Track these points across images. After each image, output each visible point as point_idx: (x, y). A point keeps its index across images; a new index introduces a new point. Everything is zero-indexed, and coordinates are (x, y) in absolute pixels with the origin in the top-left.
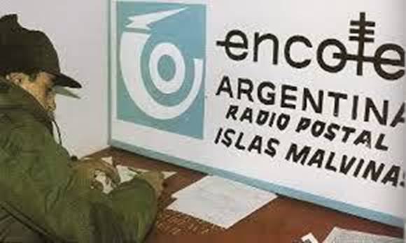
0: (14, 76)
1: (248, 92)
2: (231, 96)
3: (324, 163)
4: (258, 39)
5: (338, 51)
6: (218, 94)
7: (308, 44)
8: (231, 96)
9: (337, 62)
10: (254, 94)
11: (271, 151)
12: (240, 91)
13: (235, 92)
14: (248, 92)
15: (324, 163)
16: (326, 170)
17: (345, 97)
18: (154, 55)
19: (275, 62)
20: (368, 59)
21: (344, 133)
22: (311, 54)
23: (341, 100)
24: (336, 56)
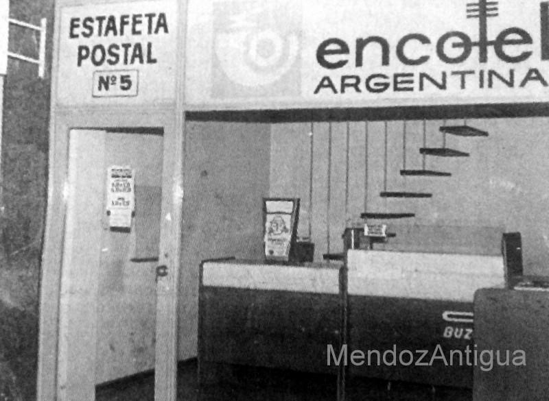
0: (325, 162)
1: (356, 86)
2: (335, 91)
3: (145, 58)
4: (361, 44)
5: (458, 40)
6: (79, 64)
7: (424, 40)
8: (335, 91)
9: (459, 52)
10: (362, 86)
11: (125, 79)
12: (344, 86)
13: (338, 86)
14: (356, 86)
15: (145, 58)
16: (149, 65)
17: (472, 72)
18: (496, 123)
19: (481, 86)
20: (475, 44)
21: (147, 19)
22: (430, 50)
23: (467, 77)
24: (455, 45)
